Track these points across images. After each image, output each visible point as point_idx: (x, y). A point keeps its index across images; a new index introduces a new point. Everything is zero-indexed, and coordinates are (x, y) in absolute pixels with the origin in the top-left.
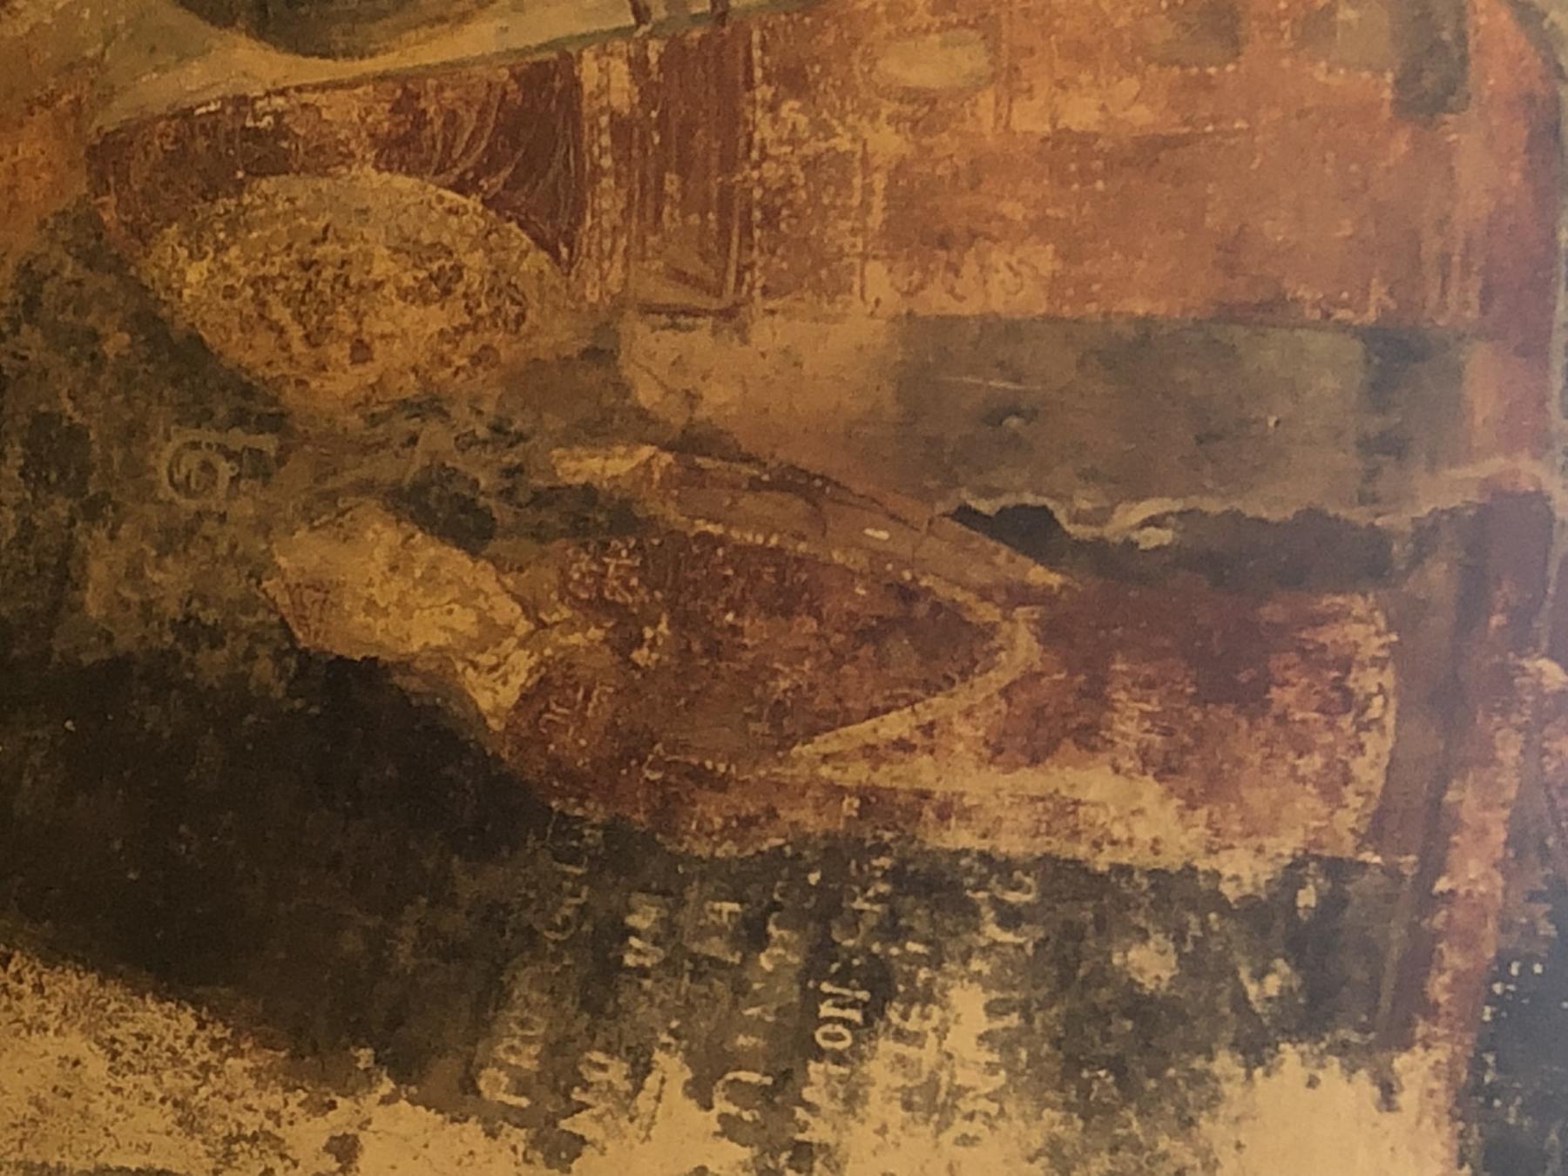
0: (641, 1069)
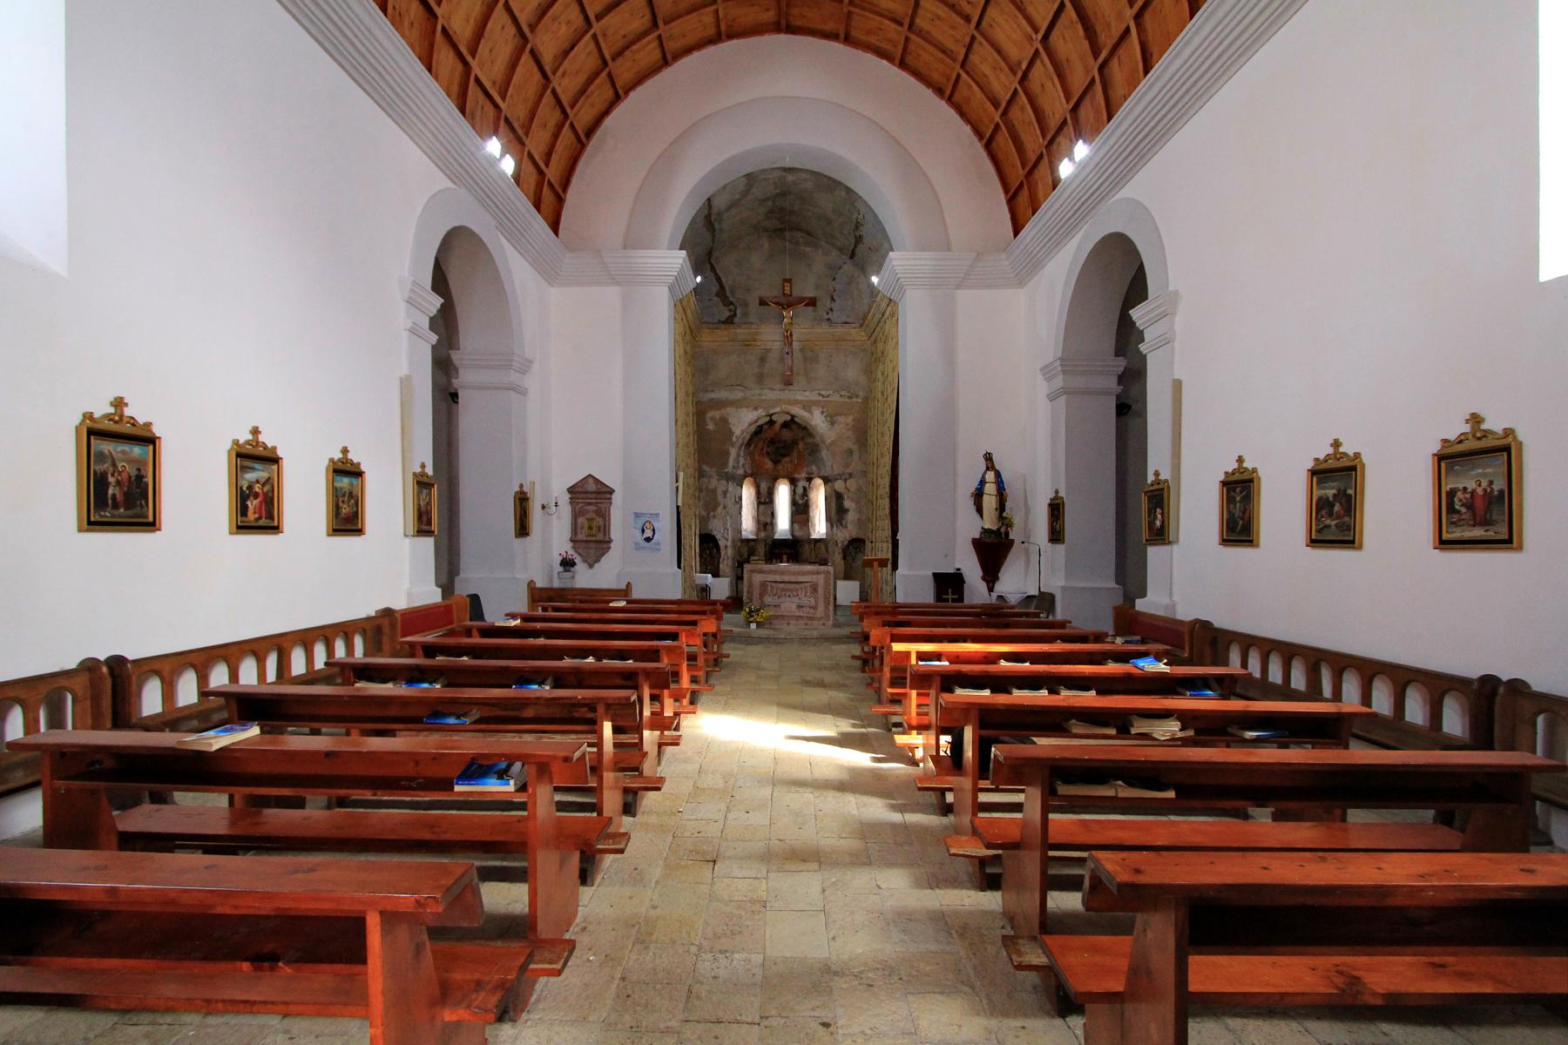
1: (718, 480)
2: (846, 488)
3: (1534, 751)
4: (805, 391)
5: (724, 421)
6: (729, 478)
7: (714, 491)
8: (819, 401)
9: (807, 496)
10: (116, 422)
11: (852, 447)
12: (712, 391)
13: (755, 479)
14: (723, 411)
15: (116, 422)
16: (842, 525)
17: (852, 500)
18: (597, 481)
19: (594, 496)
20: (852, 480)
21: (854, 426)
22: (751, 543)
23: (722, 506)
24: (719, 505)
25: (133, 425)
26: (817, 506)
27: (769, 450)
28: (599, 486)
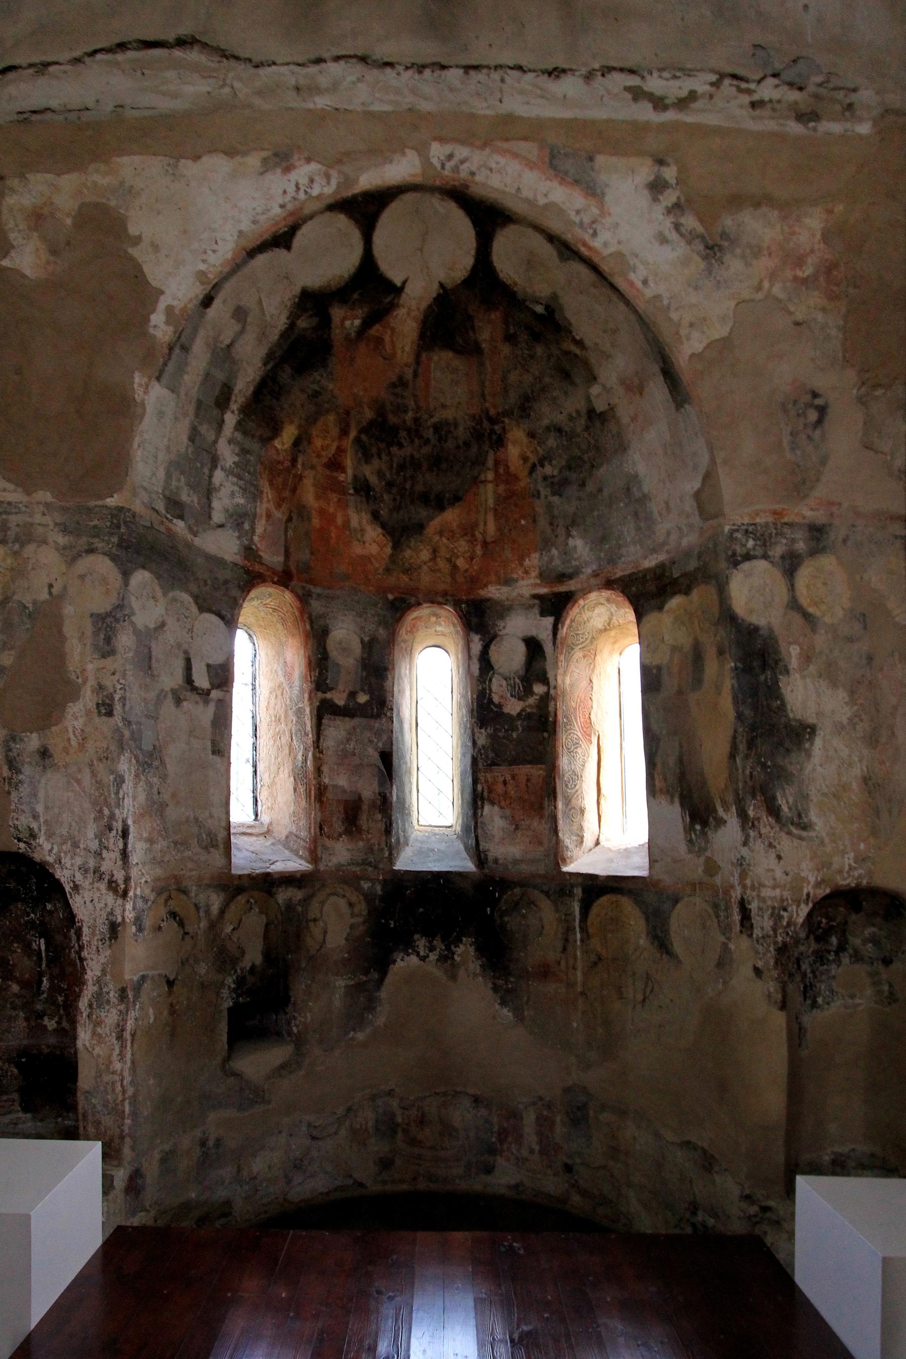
0: (237, 455)
1: (72, 556)
2: (794, 605)
4: (555, 73)
8: (640, 129)
9: (544, 679)
11: (820, 382)
13: (303, 599)
16: (774, 811)
17: (830, 674)
20: (827, 562)
21: (830, 268)
22: (283, 895)
23: (88, 698)
24: (74, 694)
26: (589, 724)
27: (369, 472)
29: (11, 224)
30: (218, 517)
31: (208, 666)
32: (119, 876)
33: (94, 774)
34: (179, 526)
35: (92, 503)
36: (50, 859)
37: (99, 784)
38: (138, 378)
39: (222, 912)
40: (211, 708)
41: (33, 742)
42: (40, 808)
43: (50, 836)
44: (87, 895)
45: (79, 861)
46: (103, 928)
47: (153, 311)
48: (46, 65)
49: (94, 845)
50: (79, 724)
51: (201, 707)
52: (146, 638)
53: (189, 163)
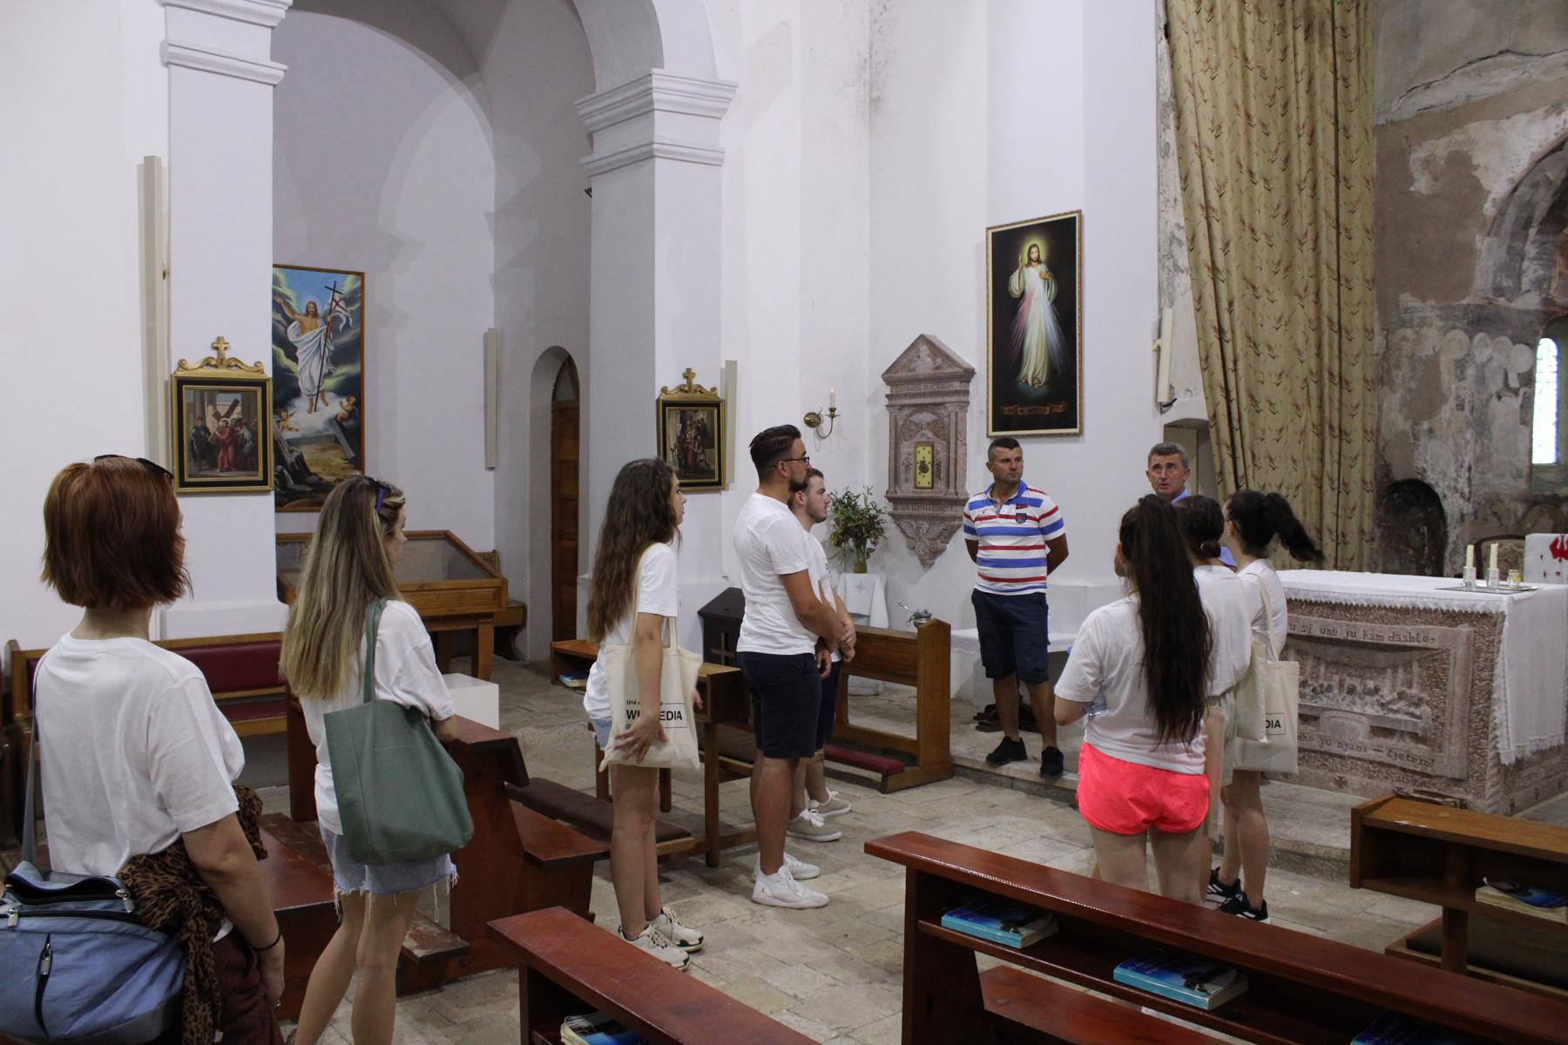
1: (1444, 331)
3: (190, 476)
5: (1460, 162)
6: (1482, 321)
7: (1432, 364)
10: (686, 392)
12: (1428, 86)
14: (1457, 136)
15: (686, 392)
18: (936, 350)
19: (930, 387)
23: (1452, 403)
24: (1444, 400)
25: (701, 392)
28: (939, 360)
29: (1414, 169)
30: (1525, 287)
31: (1519, 374)
32: (1466, 490)
33: (1454, 440)
34: (1502, 301)
35: (1455, 304)
36: (1433, 482)
37: (1457, 445)
38: (1478, 237)
39: (1525, 515)
40: (1520, 399)
41: (1425, 425)
42: (1428, 457)
43: (1433, 471)
44: (1450, 500)
45: (1446, 483)
46: (1457, 516)
47: (1486, 201)
48: (1430, 83)
49: (1454, 475)
50: (1447, 415)
51: (1514, 398)
52: (1481, 368)
53: (1505, 121)
